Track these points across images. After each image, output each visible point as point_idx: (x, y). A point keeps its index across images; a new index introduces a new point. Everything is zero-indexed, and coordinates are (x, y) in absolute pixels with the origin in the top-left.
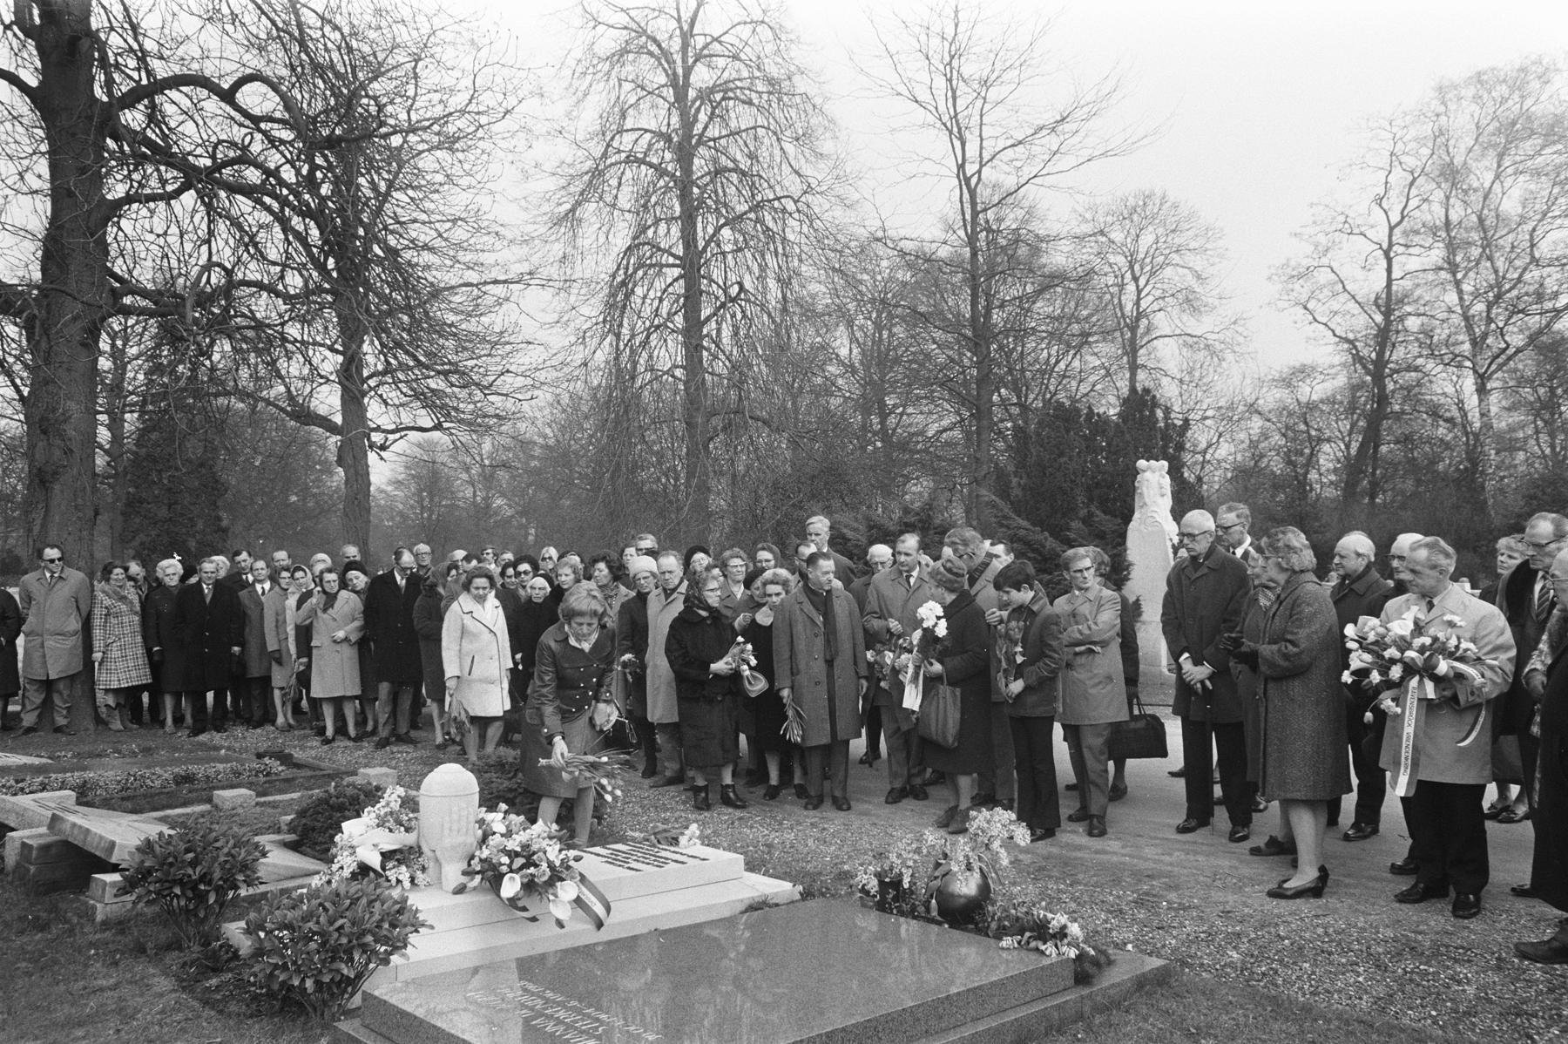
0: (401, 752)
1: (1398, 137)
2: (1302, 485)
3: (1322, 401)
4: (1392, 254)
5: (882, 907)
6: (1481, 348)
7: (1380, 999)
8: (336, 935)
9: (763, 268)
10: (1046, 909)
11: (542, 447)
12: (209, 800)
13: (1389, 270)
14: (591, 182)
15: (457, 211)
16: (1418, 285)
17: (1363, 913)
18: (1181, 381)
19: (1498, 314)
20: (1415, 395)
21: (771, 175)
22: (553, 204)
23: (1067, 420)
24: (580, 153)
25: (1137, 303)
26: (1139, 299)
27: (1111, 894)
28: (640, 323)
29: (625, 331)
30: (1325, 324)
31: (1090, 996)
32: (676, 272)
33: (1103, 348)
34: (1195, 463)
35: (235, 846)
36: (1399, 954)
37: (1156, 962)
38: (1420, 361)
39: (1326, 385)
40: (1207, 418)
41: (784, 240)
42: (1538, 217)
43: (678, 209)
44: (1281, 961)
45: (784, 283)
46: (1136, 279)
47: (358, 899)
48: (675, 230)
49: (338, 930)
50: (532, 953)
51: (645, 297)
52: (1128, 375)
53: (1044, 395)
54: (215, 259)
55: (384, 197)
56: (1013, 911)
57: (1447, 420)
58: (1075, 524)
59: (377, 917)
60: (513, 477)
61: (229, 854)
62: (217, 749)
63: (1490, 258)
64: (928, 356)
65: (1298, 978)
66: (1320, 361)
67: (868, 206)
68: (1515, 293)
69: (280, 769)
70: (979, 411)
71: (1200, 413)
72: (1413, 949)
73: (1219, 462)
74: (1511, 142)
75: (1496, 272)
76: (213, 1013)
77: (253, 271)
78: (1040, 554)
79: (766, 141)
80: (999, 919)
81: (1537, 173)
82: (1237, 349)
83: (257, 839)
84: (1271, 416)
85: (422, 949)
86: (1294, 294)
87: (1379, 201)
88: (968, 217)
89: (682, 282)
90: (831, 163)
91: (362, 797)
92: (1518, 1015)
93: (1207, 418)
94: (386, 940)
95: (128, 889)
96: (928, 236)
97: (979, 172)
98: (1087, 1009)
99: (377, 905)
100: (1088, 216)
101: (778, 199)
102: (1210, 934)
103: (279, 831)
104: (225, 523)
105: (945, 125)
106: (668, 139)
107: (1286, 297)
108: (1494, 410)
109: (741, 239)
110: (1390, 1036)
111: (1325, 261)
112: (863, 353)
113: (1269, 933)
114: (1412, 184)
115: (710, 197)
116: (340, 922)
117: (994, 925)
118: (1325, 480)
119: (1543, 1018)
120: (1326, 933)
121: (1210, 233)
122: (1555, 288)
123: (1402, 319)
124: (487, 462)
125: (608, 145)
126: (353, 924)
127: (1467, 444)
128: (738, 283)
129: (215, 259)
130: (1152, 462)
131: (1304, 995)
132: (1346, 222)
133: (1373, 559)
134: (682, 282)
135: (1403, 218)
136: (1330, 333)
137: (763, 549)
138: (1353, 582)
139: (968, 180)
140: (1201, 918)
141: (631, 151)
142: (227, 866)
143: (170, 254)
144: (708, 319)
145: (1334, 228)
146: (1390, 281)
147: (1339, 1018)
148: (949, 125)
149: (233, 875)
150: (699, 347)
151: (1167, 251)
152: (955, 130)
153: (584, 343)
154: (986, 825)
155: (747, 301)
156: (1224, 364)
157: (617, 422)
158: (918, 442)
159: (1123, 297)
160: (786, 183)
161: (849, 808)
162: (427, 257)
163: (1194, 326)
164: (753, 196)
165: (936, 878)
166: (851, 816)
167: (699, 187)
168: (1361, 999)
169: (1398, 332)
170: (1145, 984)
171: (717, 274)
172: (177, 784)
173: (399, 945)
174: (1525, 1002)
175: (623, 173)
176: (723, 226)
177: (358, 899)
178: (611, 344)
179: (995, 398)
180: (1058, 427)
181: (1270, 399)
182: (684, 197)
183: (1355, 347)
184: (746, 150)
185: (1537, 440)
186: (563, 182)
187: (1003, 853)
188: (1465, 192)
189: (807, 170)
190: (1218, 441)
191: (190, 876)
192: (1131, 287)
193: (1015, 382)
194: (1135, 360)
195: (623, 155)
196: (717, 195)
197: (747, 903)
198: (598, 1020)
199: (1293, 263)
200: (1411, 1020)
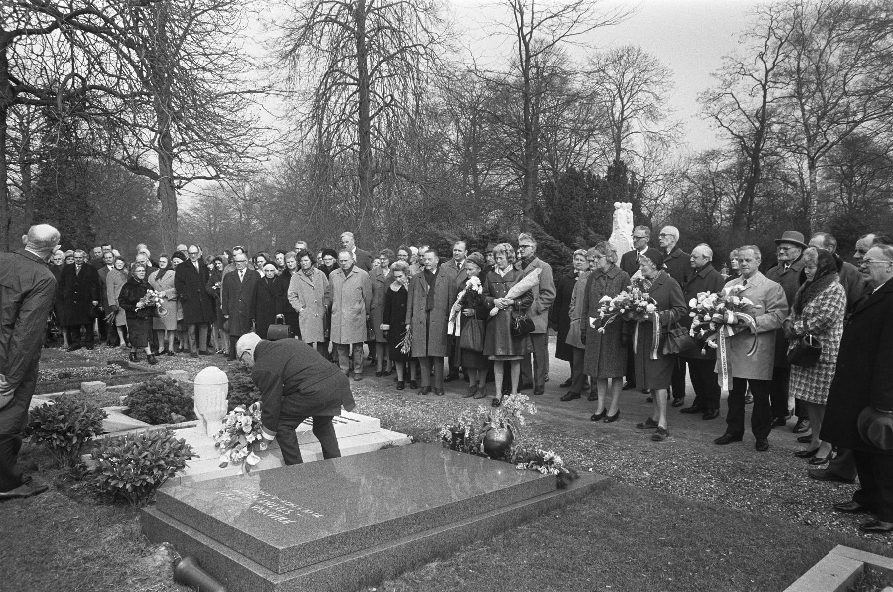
0: (191, 362)
1: (774, 18)
2: (710, 219)
3: (723, 171)
4: (767, 87)
5: (454, 447)
6: (813, 143)
7: (721, 496)
8: (143, 461)
9: (405, 86)
10: (542, 449)
11: (279, 190)
12: (79, 387)
13: (765, 97)
14: (305, 33)
15: (220, 48)
16: (780, 106)
17: (718, 451)
18: (645, 159)
19: (823, 124)
20: (775, 169)
21: (411, 31)
22: (282, 45)
23: (576, 179)
24: (298, 15)
25: (622, 113)
26: (623, 110)
27: (583, 442)
28: (333, 117)
29: (325, 122)
30: (727, 127)
31: (565, 495)
32: (355, 88)
33: (602, 138)
34: (651, 206)
35: (88, 412)
36: (734, 473)
37: (603, 478)
38: (779, 150)
39: (726, 162)
40: (659, 180)
41: (418, 70)
42: (849, 67)
43: (355, 50)
44: (671, 477)
45: (418, 96)
46: (622, 99)
47: (156, 441)
48: (354, 63)
49: (144, 458)
50: (887, 558)
51: (336, 102)
52: (615, 154)
53: (567, 164)
54: (76, 71)
55: (183, 38)
56: (525, 450)
57: (792, 184)
58: (579, 238)
59: (166, 450)
60: (262, 208)
61: (84, 416)
62: (85, 359)
63: (821, 91)
64: (501, 141)
65: (680, 486)
66: (724, 148)
67: (467, 52)
68: (833, 111)
69: (121, 370)
70: (527, 171)
71: (655, 177)
72: (742, 470)
73: (664, 205)
74: (837, 22)
75: (824, 99)
76: (74, 503)
77: (100, 80)
78: (559, 255)
79: (408, 10)
80: (517, 454)
81: (850, 41)
82: (677, 140)
83: (104, 409)
84: (694, 180)
85: (194, 469)
86: (711, 109)
87: (761, 56)
88: (524, 58)
89: (358, 94)
90: (446, 25)
91: (165, 386)
92: (792, 503)
93: (659, 180)
94: (172, 463)
95: (26, 435)
96: (501, 70)
97: (531, 32)
98: (563, 502)
99: (167, 444)
100: (596, 61)
101: (415, 46)
102: (635, 463)
103: (119, 405)
104: (93, 231)
105: (511, 3)
106: (350, 9)
107: (706, 111)
108: (818, 179)
109: (392, 69)
110: (724, 515)
111: (729, 90)
112: (465, 138)
113: (667, 462)
114: (781, 45)
115: (374, 44)
116: (146, 453)
117: (514, 458)
118: (723, 216)
119: (804, 504)
120: (697, 463)
121: (665, 73)
122: (855, 109)
123: (770, 125)
124: (247, 198)
125: (315, 11)
126: (153, 454)
127: (803, 198)
128: (391, 95)
129: (76, 71)
130: (623, 204)
131: (682, 494)
132: (742, 68)
133: (711, 259)
134: (358, 94)
135: (774, 66)
136: (730, 132)
137: (403, 249)
138: (698, 272)
139: (524, 37)
140: (631, 454)
141: (328, 14)
142: (84, 423)
143: (47, 68)
144: (373, 117)
145: (735, 71)
146: (765, 102)
147: (699, 506)
148: (514, 4)
149: (87, 428)
150: (367, 133)
151: (640, 83)
152: (518, 7)
153: (301, 129)
154: (512, 403)
155: (396, 106)
156: (669, 149)
157: (321, 175)
158: (495, 191)
159: (614, 109)
160: (419, 36)
161: (443, 394)
162: (208, 75)
163: (653, 127)
164: (400, 43)
165: (484, 432)
166: (444, 398)
167: (368, 37)
168: (712, 496)
169: (767, 133)
170: (594, 489)
171: (379, 91)
172: (61, 378)
173: (181, 466)
174: (796, 497)
175: (324, 28)
176: (382, 61)
177: (156, 441)
178: (316, 130)
179: (539, 166)
180: (571, 182)
181: (694, 170)
182: (360, 44)
183: (743, 141)
184: (396, 16)
185: (841, 196)
186: (288, 33)
187: (522, 419)
188: (810, 52)
189: (432, 29)
190: (664, 194)
191: (61, 428)
192: (618, 102)
193: (550, 156)
194: (619, 145)
195: (324, 17)
196: (379, 43)
197: (381, 446)
198: (288, 506)
199: (711, 91)
200: (737, 507)
